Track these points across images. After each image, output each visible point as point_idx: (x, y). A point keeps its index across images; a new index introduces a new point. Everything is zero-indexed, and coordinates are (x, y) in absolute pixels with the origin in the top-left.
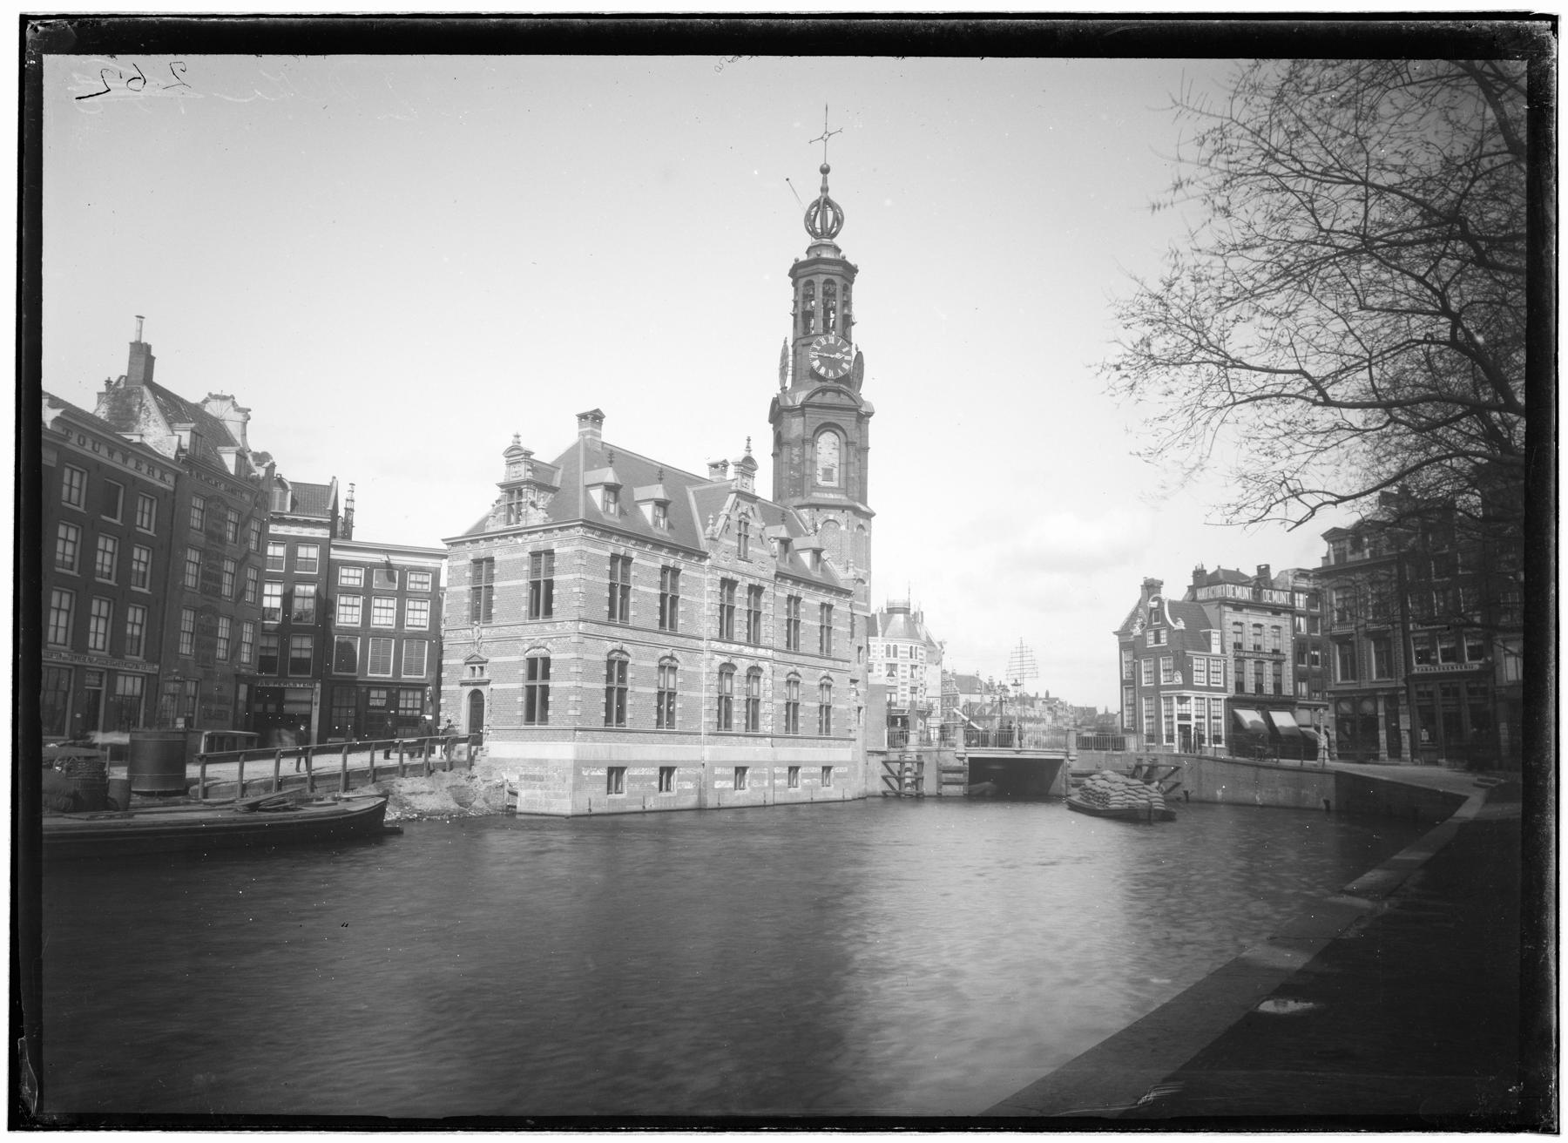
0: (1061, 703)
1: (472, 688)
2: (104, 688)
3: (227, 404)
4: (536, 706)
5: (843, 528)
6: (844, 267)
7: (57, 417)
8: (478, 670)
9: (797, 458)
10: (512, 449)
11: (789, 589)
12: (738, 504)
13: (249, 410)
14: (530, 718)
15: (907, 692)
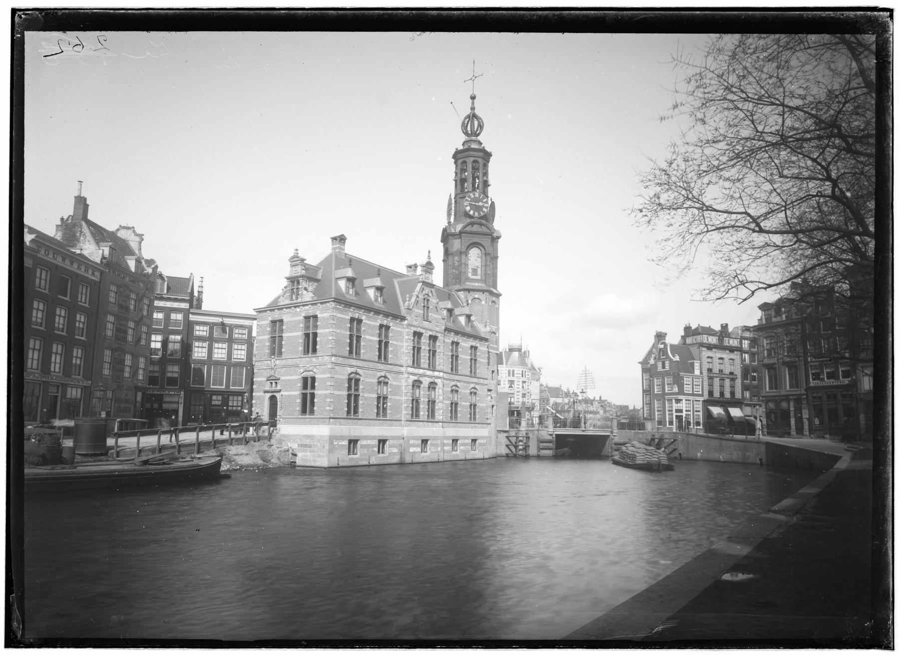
0: (608, 403)
1: (271, 394)
2: (59, 394)
3: (130, 231)
4: (307, 404)
5: (483, 302)
6: (484, 153)
7: (33, 239)
8: (274, 384)
9: (457, 263)
10: (293, 257)
11: (452, 337)
12: (423, 289)
13: (143, 235)
14: (304, 411)
15: (520, 397)
